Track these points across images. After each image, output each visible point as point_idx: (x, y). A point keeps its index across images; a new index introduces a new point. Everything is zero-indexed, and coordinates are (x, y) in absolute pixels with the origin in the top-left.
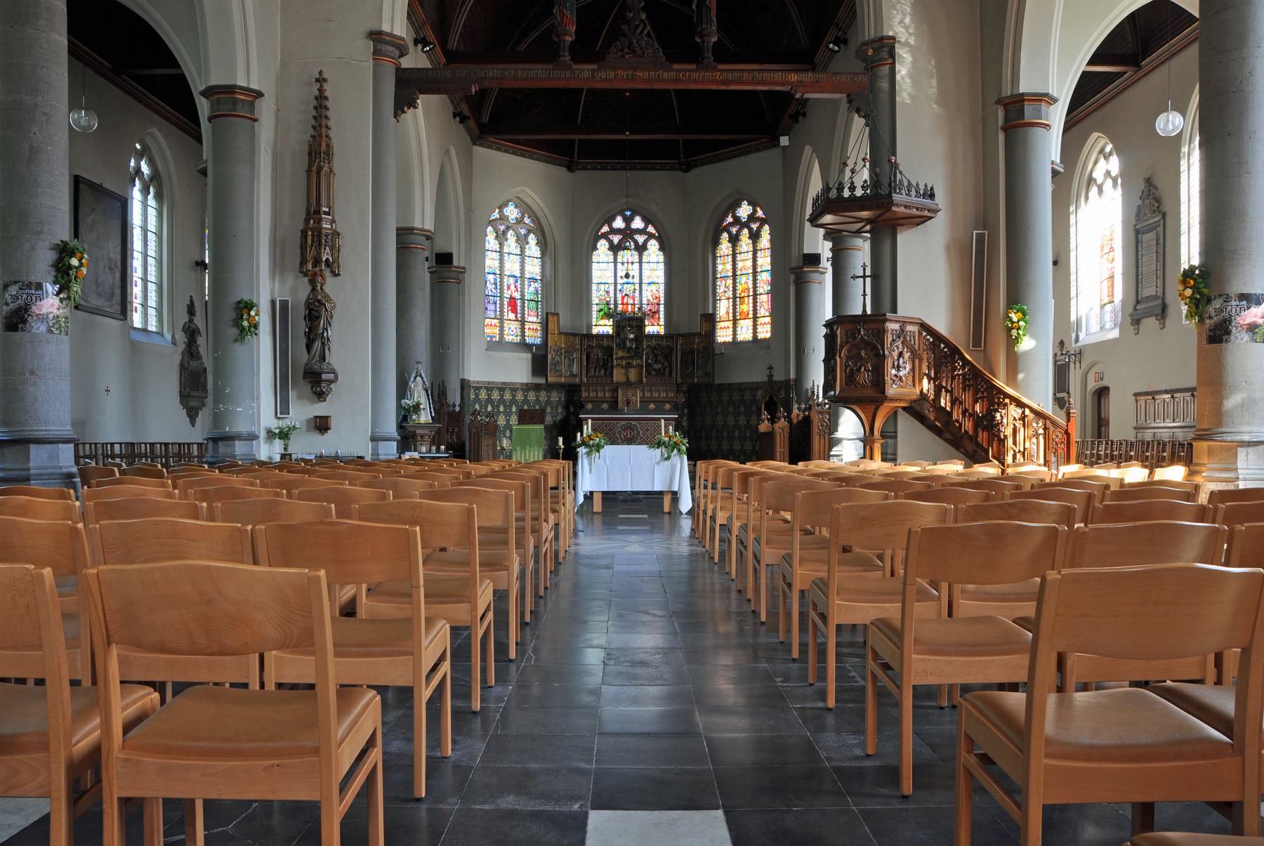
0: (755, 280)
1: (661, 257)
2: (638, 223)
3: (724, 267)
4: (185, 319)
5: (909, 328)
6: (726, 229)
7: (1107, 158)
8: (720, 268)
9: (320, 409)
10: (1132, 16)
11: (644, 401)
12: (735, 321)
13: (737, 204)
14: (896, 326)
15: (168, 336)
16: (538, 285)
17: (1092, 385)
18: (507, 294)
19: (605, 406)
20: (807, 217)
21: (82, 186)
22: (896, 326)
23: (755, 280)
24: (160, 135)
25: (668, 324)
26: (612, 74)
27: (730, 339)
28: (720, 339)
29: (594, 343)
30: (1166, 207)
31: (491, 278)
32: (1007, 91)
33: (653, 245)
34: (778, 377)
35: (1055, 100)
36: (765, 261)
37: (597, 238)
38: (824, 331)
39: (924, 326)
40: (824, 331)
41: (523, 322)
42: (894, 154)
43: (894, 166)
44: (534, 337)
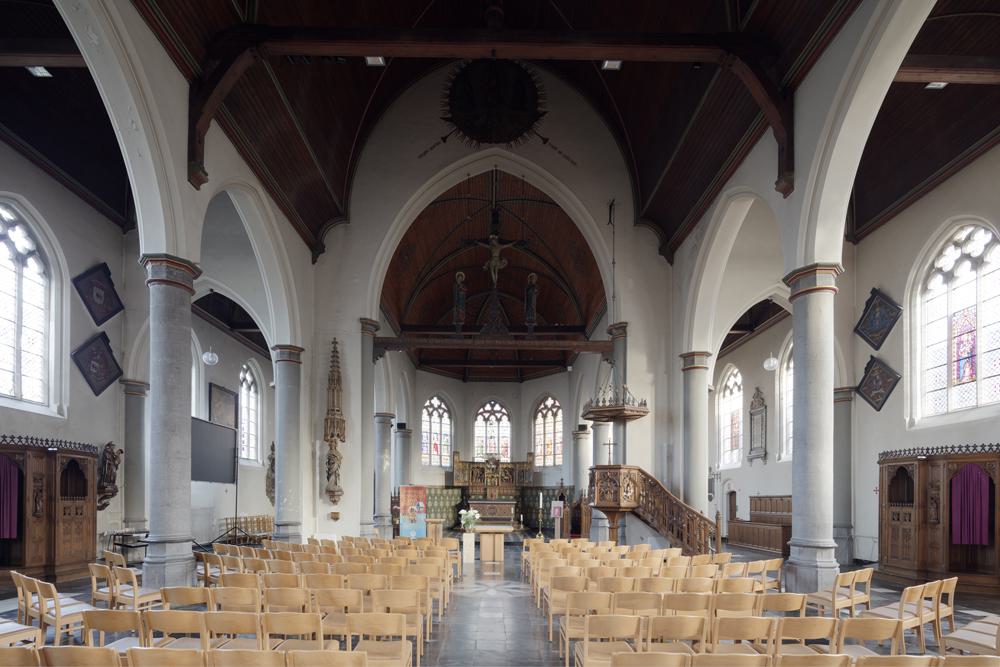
0: (555, 437)
1: (508, 424)
2: (497, 407)
3: (539, 429)
4: (270, 453)
5: (634, 472)
6: (541, 411)
7: (735, 376)
8: (537, 430)
9: (334, 509)
10: (751, 309)
11: (500, 495)
12: (545, 456)
13: (546, 399)
14: (626, 471)
15: (260, 462)
16: (449, 438)
17: (726, 490)
18: (433, 442)
19: (481, 497)
20: (581, 414)
21: (213, 389)
22: (626, 471)
23: (555, 437)
24: (254, 363)
25: (512, 458)
26: (483, 342)
27: (542, 465)
28: (537, 465)
29: (476, 466)
30: (767, 403)
31: (424, 434)
32: (685, 351)
33: (505, 418)
34: (567, 484)
35: (711, 355)
36: (560, 427)
37: (477, 415)
38: (589, 472)
39: (640, 470)
40: (589, 472)
41: (441, 456)
42: (625, 382)
43: (625, 389)
44: (447, 463)
